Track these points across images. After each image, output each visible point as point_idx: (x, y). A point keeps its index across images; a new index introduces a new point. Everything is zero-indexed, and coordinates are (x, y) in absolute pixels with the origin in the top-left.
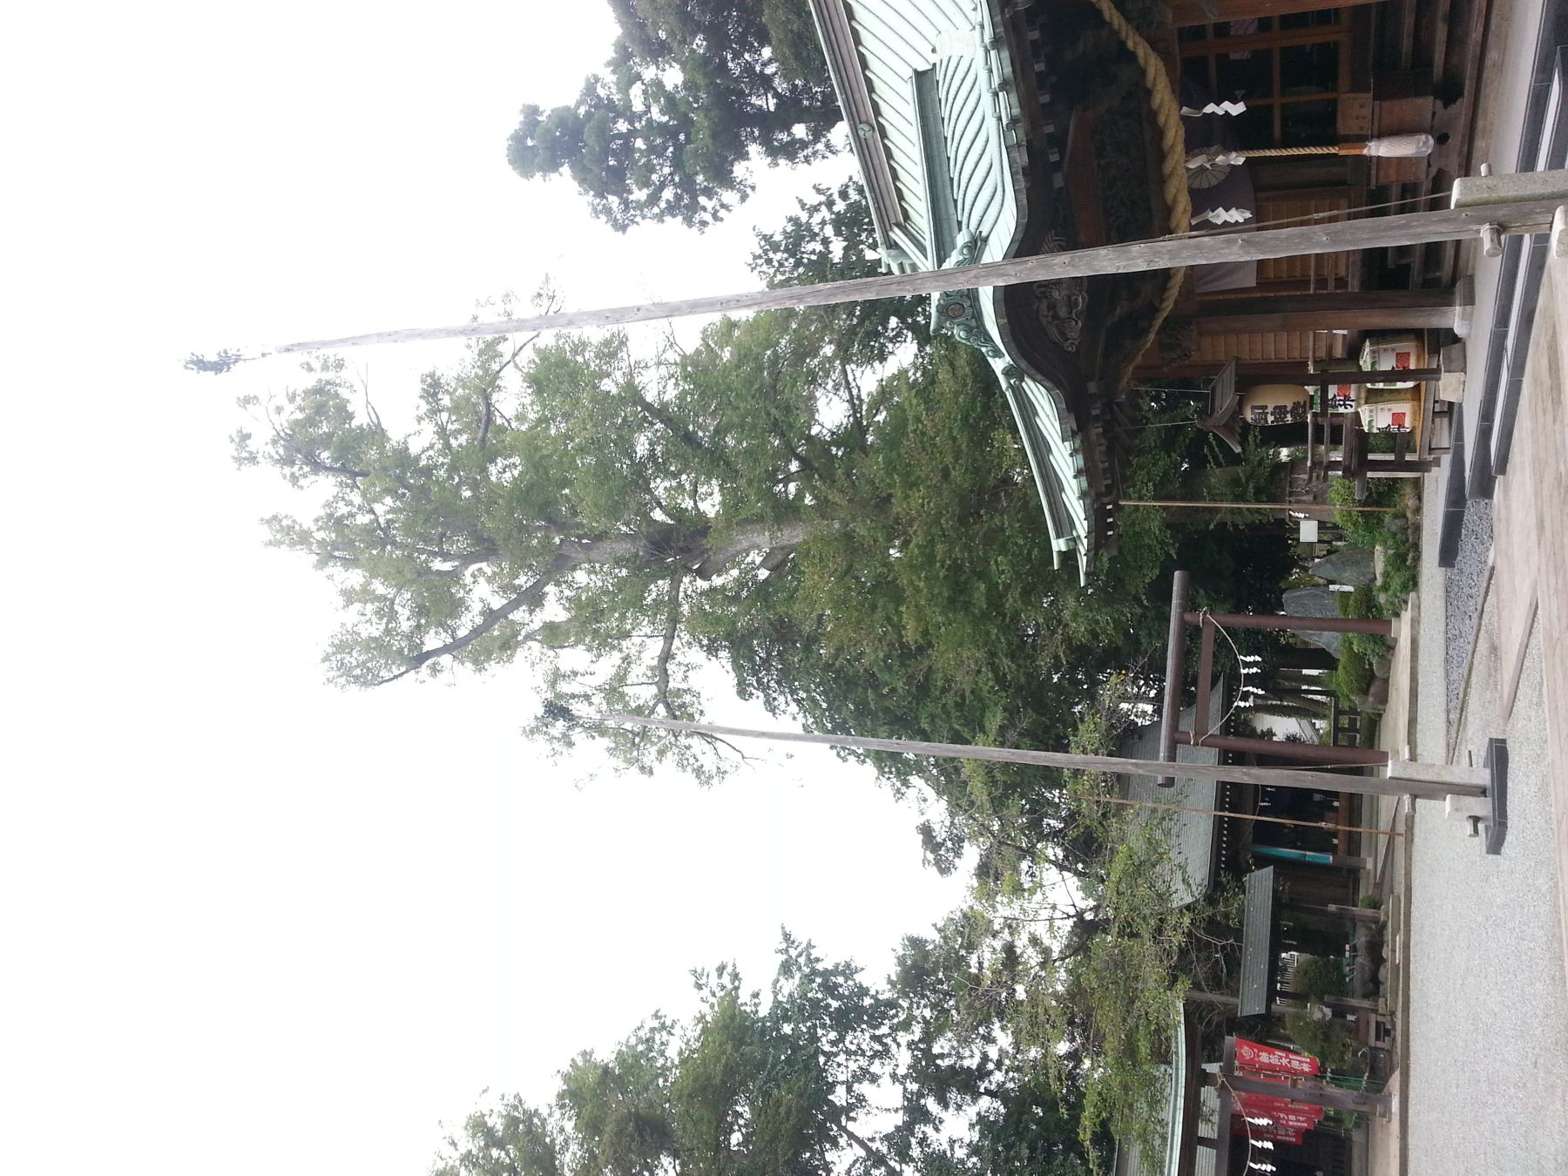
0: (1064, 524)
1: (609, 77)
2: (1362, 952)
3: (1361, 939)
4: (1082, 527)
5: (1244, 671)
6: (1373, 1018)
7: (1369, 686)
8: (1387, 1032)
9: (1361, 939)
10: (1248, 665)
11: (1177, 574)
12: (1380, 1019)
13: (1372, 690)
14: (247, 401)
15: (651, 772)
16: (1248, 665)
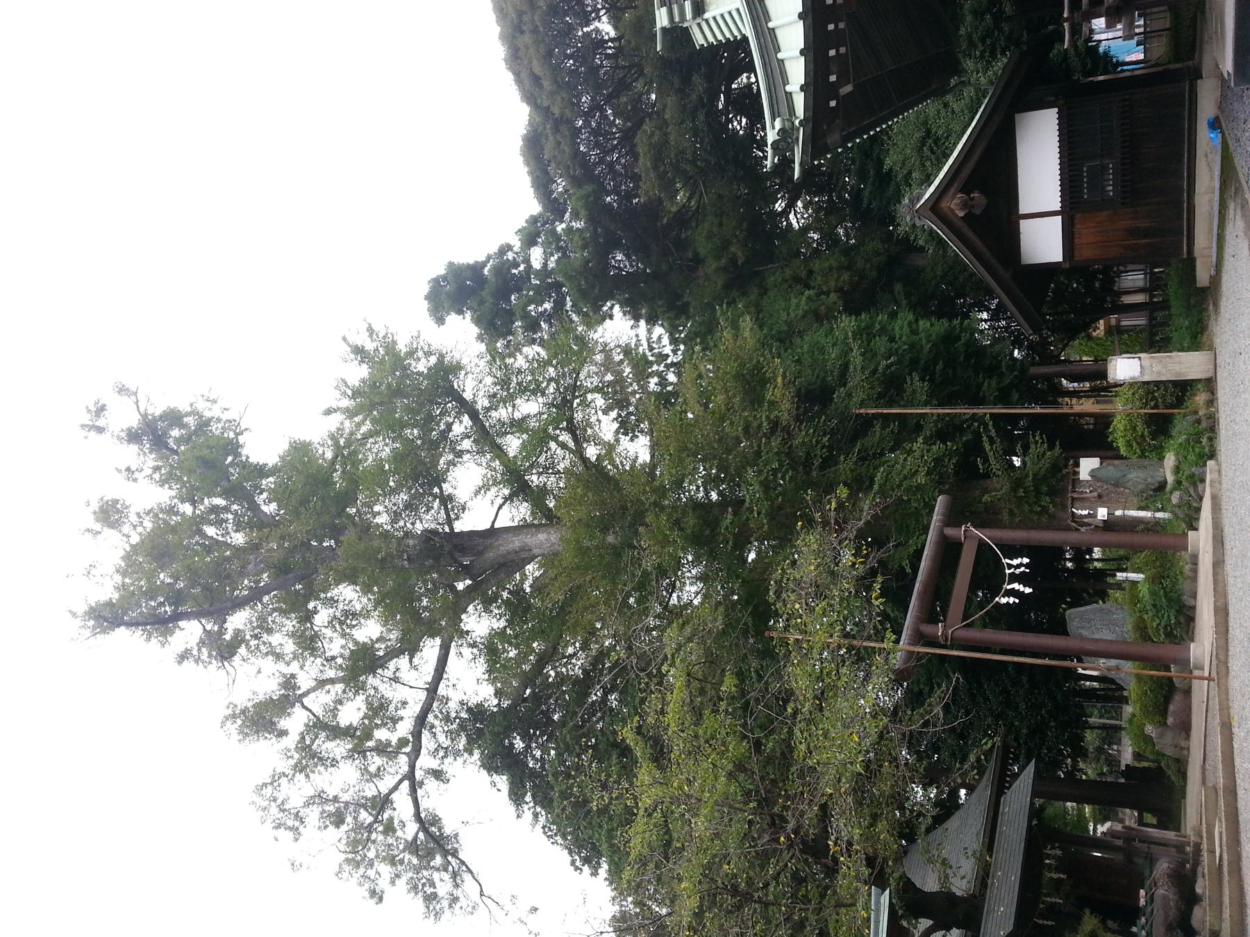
0: (782, 103)
1: (517, 245)
3: (1163, 866)
9: (1163, 866)
14: (122, 390)
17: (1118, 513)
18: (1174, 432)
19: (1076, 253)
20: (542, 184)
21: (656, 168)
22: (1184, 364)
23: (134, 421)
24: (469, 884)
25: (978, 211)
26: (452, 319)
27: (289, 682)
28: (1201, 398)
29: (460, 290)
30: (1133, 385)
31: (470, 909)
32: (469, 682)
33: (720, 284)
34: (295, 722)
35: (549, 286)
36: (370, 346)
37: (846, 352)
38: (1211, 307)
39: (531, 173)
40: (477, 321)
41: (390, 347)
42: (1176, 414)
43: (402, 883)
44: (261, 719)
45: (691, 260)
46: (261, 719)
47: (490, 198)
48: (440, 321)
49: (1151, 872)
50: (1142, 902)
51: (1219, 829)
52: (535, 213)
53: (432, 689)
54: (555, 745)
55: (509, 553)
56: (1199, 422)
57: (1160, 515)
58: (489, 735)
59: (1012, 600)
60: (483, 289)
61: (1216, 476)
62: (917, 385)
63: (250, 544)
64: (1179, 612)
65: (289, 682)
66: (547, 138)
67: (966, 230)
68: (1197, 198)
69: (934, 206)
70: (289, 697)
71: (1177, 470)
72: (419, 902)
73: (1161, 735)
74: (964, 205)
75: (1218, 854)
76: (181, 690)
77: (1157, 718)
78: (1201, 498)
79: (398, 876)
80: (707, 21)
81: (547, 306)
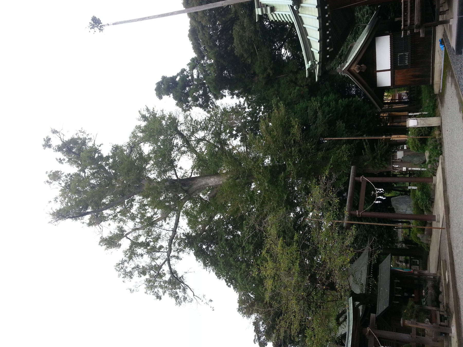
0: (310, 56)
1: (188, 69)
3: (430, 284)
4: (317, 57)
6: (438, 313)
9: (430, 284)
11: (352, 167)
12: (441, 313)
14: (55, 132)
15: (160, 299)
17: (410, 169)
18: (428, 143)
19: (395, 83)
20: (196, 48)
21: (241, 43)
22: (433, 121)
23: (60, 143)
24: (188, 291)
25: (363, 71)
26: (165, 97)
27: (121, 229)
28: (437, 132)
29: (167, 86)
30: (414, 128)
31: (190, 301)
32: (184, 226)
33: (264, 83)
34: (125, 243)
35: (201, 85)
36: (147, 115)
37: (316, 112)
38: (439, 100)
39: (193, 44)
40: (175, 98)
41: (154, 115)
42: (430, 140)
43: (167, 294)
44: (111, 242)
45: (252, 74)
46: (111, 242)
47: (177, 52)
48: (160, 98)
49: (426, 285)
50: (424, 294)
51: (448, 275)
52: (194, 57)
53: (174, 231)
54: (227, 250)
55: (201, 186)
56: (436, 141)
57: (423, 169)
58: (190, 241)
59: (379, 202)
60: (177, 86)
61: (443, 161)
62: (340, 125)
63: (103, 184)
64: (429, 200)
65: (121, 229)
66: (199, 32)
67: (359, 77)
68: (435, 65)
69: (349, 69)
70: (121, 234)
71: (430, 157)
72: (173, 300)
73: (422, 237)
74: (359, 69)
75: (447, 281)
76: (83, 234)
77: (422, 232)
78: (437, 167)
79: (165, 292)
80: (275, 14)
81: (201, 92)
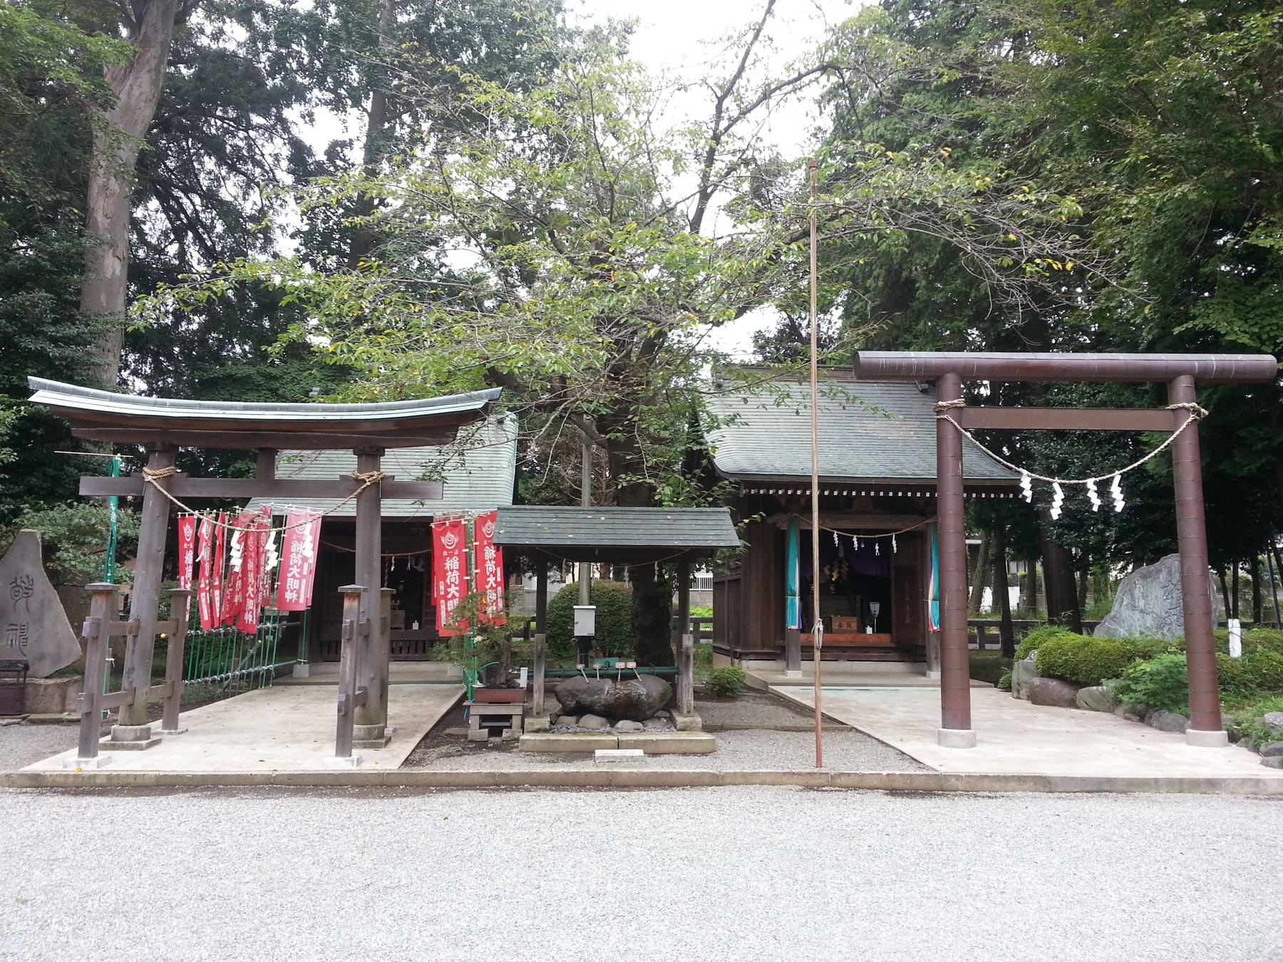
2: (622, 689)
3: (646, 687)
5: (1090, 483)
6: (516, 710)
7: (1061, 678)
8: (496, 732)
9: (646, 687)
10: (1103, 489)
12: (516, 721)
13: (1053, 684)
16: (1103, 489)
